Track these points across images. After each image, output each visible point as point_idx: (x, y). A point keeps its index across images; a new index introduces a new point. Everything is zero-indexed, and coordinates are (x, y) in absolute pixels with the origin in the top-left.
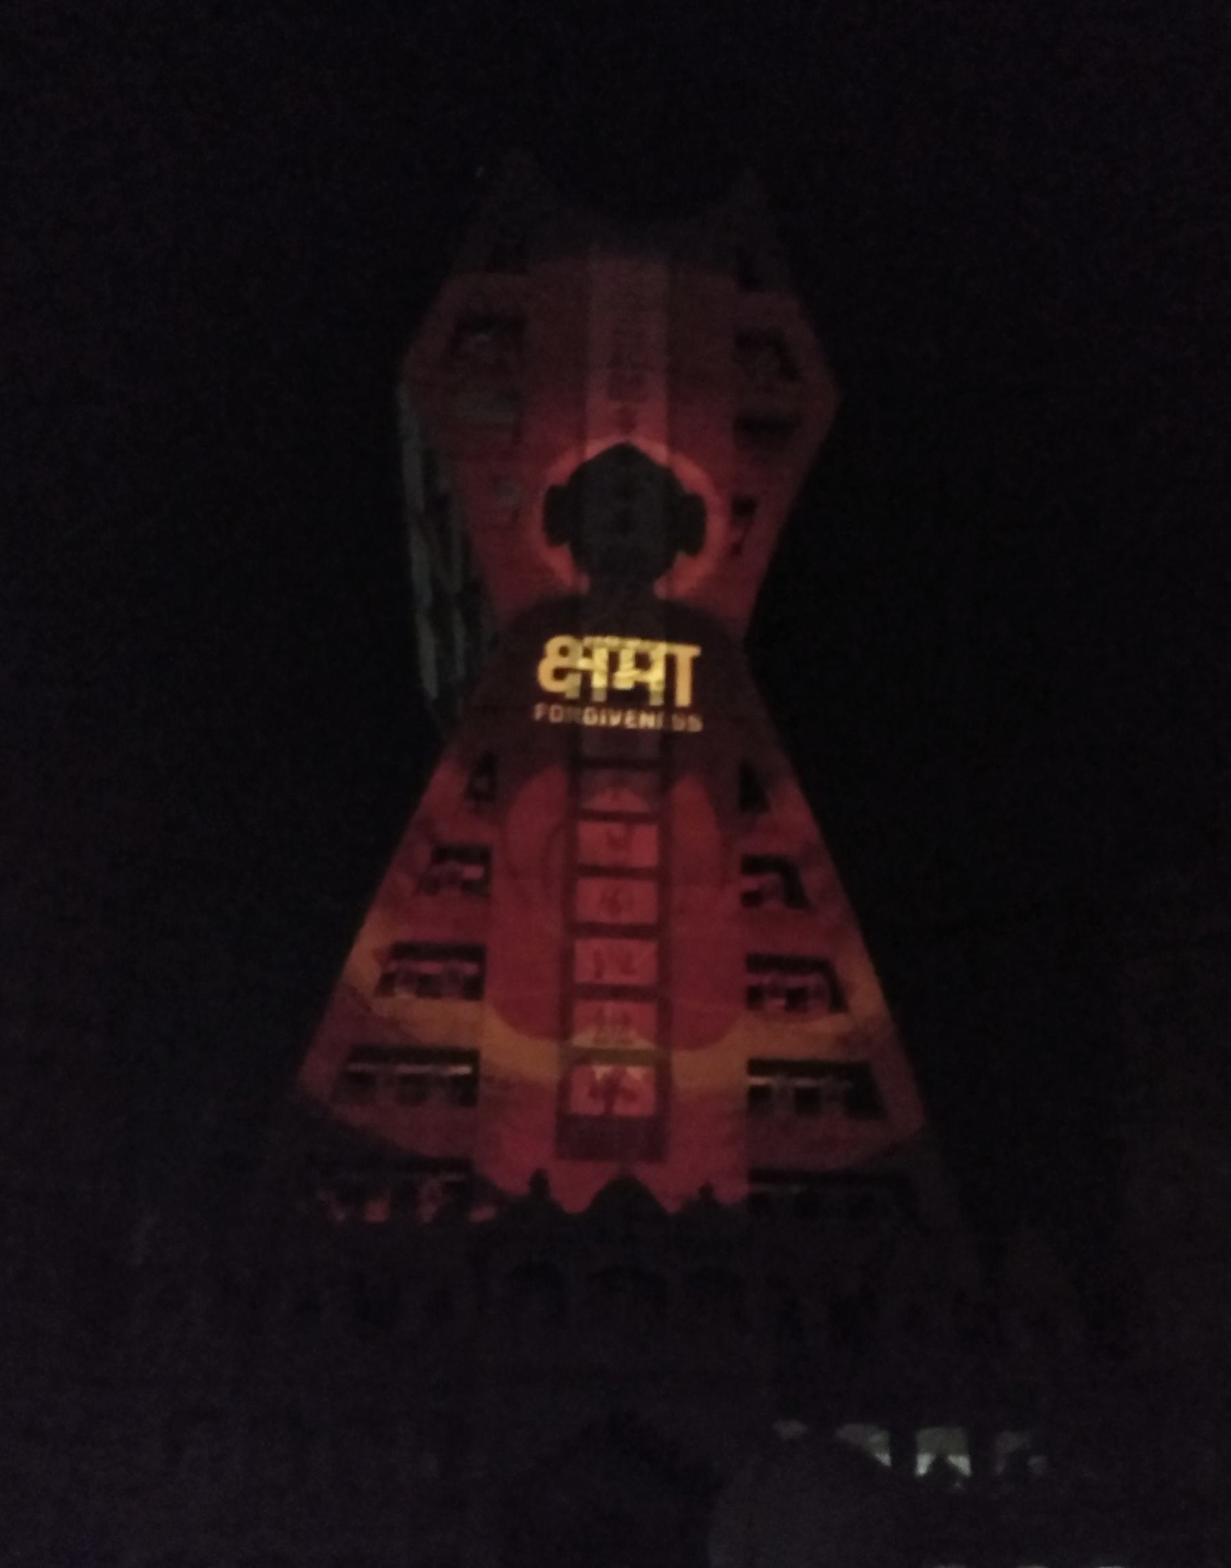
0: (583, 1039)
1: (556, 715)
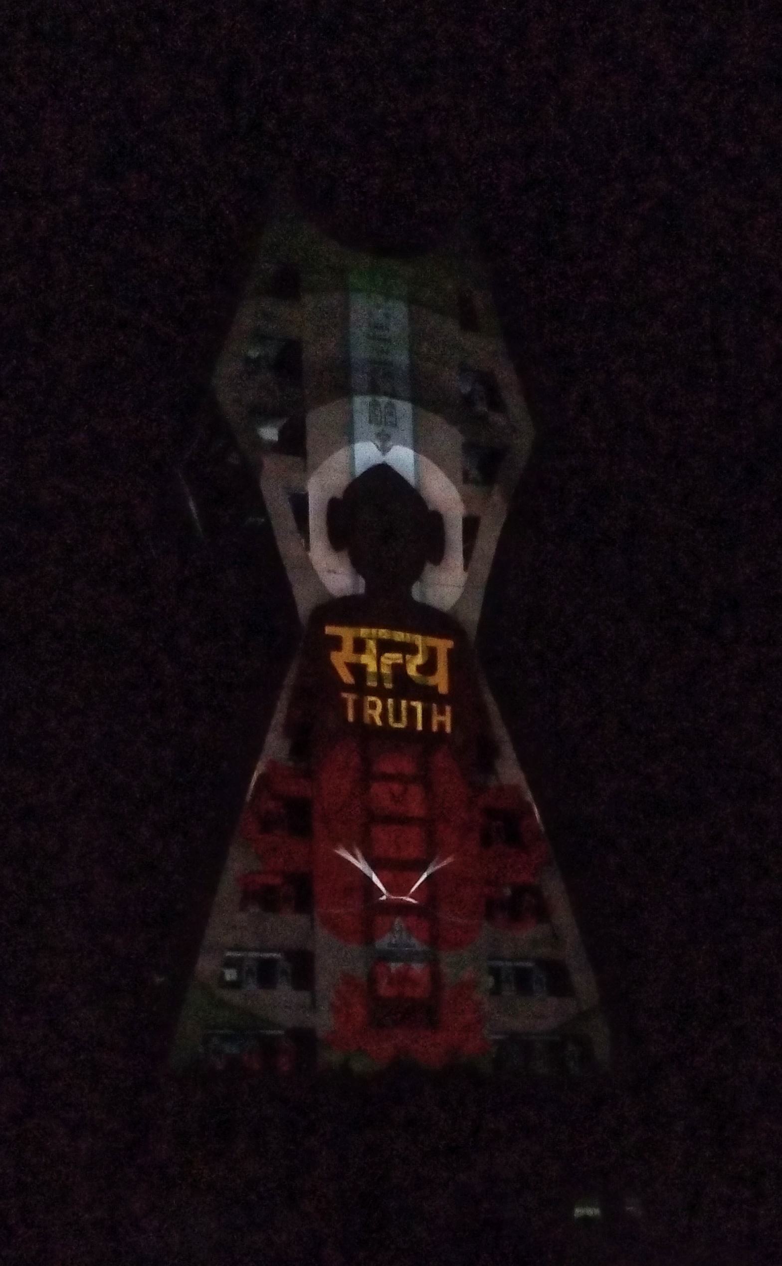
0: (384, 943)
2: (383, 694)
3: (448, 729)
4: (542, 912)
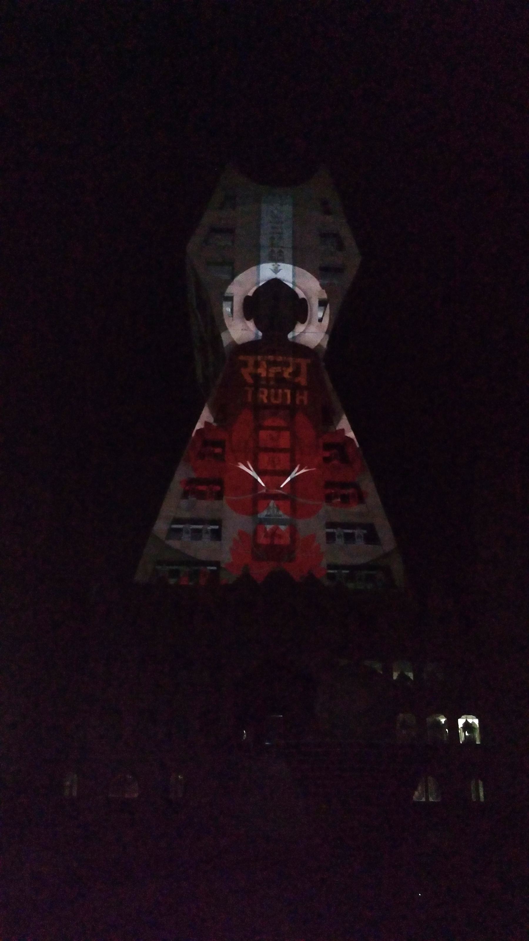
0: (263, 514)
1: (477, 735)
2: (268, 387)
3: (306, 402)
4: (361, 498)
